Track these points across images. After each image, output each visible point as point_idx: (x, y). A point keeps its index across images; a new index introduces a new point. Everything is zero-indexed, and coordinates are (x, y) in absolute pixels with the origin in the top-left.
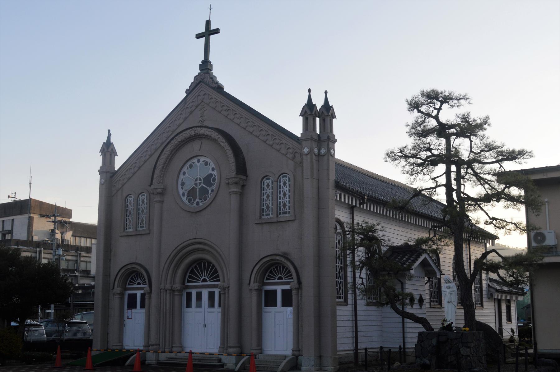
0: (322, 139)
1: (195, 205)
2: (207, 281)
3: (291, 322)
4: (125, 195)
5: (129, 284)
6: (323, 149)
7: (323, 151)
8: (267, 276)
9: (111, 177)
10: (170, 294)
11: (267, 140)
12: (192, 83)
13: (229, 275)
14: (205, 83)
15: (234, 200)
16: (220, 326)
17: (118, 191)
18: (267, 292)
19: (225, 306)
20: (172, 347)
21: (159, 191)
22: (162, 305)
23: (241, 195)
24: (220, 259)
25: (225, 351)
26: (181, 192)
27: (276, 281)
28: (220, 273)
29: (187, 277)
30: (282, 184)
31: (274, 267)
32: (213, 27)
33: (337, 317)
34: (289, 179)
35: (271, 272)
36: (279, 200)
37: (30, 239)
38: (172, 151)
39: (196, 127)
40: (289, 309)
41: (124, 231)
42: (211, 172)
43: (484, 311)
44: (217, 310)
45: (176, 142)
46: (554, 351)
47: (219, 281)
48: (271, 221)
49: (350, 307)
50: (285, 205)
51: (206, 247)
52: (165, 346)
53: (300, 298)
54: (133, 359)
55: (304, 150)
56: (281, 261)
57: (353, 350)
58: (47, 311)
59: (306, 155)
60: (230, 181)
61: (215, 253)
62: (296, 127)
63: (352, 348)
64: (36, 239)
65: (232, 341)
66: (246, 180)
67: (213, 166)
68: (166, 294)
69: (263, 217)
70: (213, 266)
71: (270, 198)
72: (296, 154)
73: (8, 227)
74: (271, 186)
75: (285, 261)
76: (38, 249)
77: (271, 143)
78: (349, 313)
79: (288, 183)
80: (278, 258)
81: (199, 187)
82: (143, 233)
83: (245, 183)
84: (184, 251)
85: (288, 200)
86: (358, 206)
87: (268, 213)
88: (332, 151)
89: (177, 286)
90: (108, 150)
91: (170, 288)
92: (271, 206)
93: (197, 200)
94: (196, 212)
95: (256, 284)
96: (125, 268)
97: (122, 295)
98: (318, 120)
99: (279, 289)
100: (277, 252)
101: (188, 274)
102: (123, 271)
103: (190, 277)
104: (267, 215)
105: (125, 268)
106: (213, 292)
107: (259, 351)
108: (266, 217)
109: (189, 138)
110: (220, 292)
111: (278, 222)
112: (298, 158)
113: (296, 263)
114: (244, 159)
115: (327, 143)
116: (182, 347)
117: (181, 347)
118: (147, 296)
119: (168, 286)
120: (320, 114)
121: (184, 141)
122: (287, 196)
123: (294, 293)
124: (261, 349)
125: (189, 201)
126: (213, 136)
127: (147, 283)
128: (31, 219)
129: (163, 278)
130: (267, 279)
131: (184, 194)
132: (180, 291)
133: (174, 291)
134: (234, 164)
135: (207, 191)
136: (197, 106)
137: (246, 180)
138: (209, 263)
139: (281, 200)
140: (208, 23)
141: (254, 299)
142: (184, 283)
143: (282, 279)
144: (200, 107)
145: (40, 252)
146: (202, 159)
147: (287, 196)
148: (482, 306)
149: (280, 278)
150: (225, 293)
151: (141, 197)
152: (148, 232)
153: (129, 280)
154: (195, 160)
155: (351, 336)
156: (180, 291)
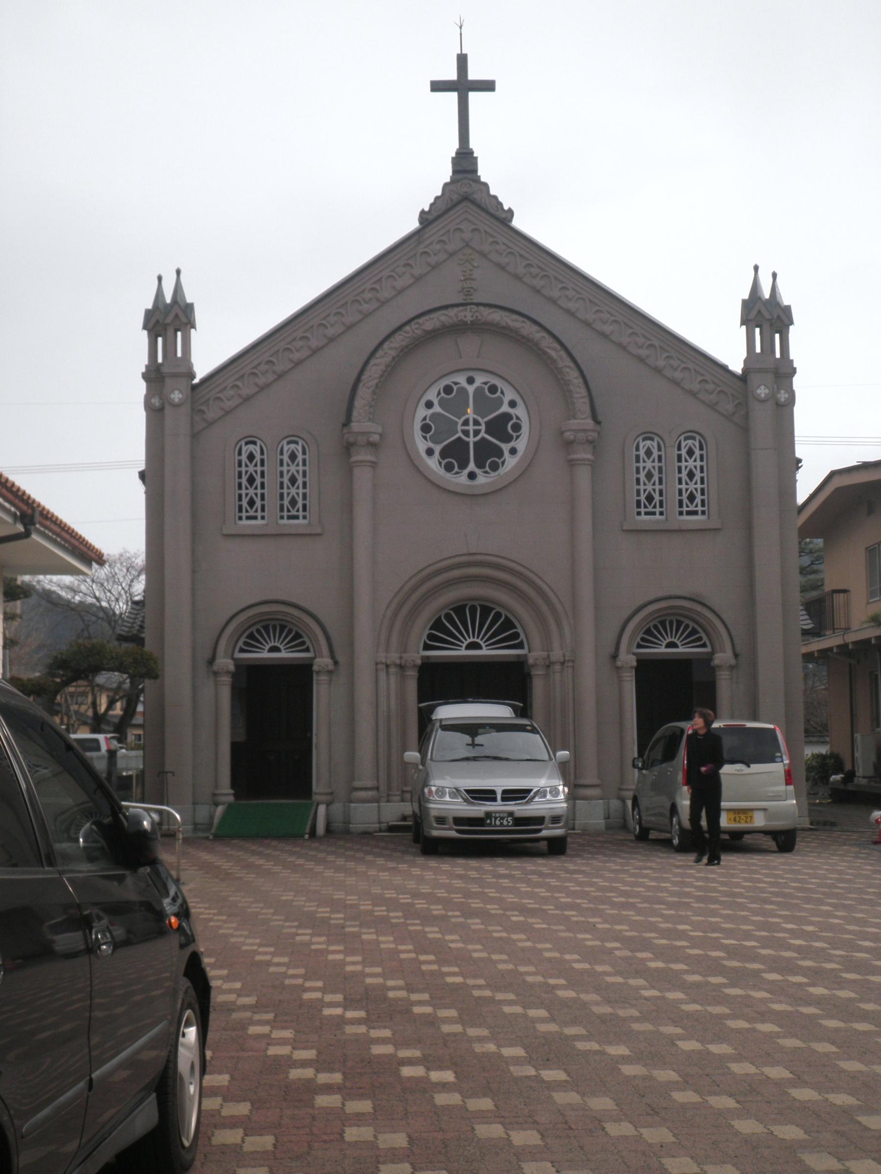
12: (437, 198)
14: (466, 202)
38: (402, 350)
45: (418, 332)
50: (692, 498)
55: (759, 391)
81: (472, 440)
90: (169, 319)
102: (663, 604)
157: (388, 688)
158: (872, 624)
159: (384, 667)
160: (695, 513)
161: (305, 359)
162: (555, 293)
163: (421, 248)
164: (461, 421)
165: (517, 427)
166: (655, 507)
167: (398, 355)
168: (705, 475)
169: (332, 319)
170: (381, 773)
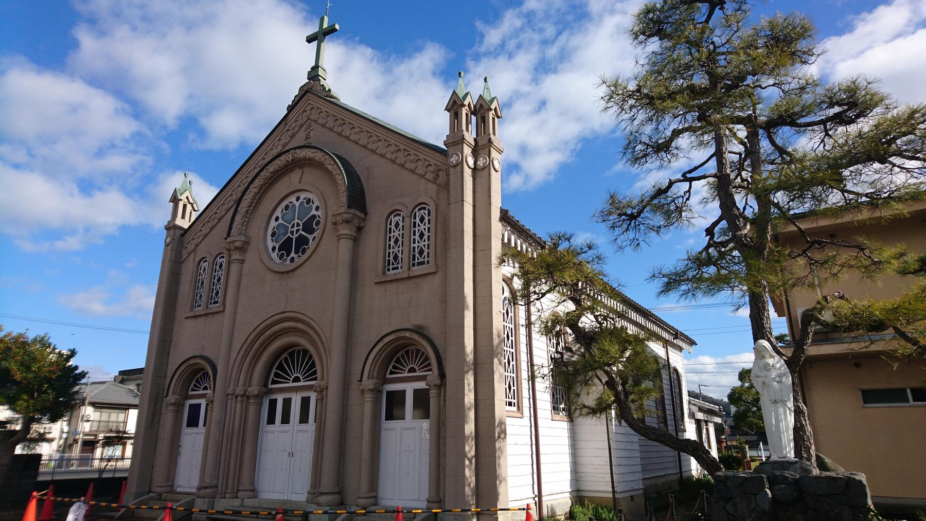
2: (300, 381)
3: (426, 445)
4: (198, 259)
5: (193, 390)
7: (481, 163)
8: (391, 367)
9: (182, 235)
10: (242, 402)
13: (331, 368)
15: (345, 247)
17: (189, 254)
18: (390, 394)
20: (238, 491)
21: (238, 244)
22: (227, 420)
23: (356, 240)
24: (319, 343)
26: (270, 245)
27: (406, 374)
28: (318, 367)
29: (272, 375)
30: (417, 220)
31: (402, 352)
35: (398, 361)
36: (412, 245)
38: (261, 188)
39: (295, 148)
41: (192, 310)
42: (314, 212)
46: (894, 501)
47: (315, 379)
49: (526, 421)
50: (421, 252)
51: (300, 326)
52: (226, 489)
53: (442, 403)
59: (455, 166)
60: (339, 218)
65: (327, 483)
67: (317, 203)
68: (236, 401)
69: (388, 273)
70: (311, 357)
71: (400, 242)
72: (441, 173)
75: (420, 340)
80: (408, 334)
82: (215, 310)
85: (426, 243)
87: (396, 266)
89: (254, 389)
91: (242, 393)
93: (293, 255)
94: (288, 272)
95: (371, 381)
97: (179, 406)
100: (408, 326)
101: (274, 371)
102: (182, 368)
103: (276, 375)
104: (393, 269)
106: (309, 398)
107: (372, 500)
108: (391, 272)
109: (286, 166)
111: (409, 278)
113: (437, 343)
114: (363, 190)
116: (254, 492)
117: (254, 491)
119: (239, 390)
120: (478, 107)
123: (433, 393)
124: (376, 497)
125: (281, 257)
126: (317, 158)
129: (233, 376)
131: (274, 249)
132: (260, 397)
133: (248, 397)
134: (345, 194)
135: (306, 241)
138: (306, 351)
139: (416, 245)
141: (368, 407)
142: (266, 385)
143: (415, 371)
144: (305, 126)
146: (303, 196)
147: (426, 237)
149: (412, 370)
151: (219, 260)
152: (221, 309)
154: (293, 199)
156: (260, 397)
160: (423, 263)
162: (347, 132)
165: (318, 223)
168: (412, 237)
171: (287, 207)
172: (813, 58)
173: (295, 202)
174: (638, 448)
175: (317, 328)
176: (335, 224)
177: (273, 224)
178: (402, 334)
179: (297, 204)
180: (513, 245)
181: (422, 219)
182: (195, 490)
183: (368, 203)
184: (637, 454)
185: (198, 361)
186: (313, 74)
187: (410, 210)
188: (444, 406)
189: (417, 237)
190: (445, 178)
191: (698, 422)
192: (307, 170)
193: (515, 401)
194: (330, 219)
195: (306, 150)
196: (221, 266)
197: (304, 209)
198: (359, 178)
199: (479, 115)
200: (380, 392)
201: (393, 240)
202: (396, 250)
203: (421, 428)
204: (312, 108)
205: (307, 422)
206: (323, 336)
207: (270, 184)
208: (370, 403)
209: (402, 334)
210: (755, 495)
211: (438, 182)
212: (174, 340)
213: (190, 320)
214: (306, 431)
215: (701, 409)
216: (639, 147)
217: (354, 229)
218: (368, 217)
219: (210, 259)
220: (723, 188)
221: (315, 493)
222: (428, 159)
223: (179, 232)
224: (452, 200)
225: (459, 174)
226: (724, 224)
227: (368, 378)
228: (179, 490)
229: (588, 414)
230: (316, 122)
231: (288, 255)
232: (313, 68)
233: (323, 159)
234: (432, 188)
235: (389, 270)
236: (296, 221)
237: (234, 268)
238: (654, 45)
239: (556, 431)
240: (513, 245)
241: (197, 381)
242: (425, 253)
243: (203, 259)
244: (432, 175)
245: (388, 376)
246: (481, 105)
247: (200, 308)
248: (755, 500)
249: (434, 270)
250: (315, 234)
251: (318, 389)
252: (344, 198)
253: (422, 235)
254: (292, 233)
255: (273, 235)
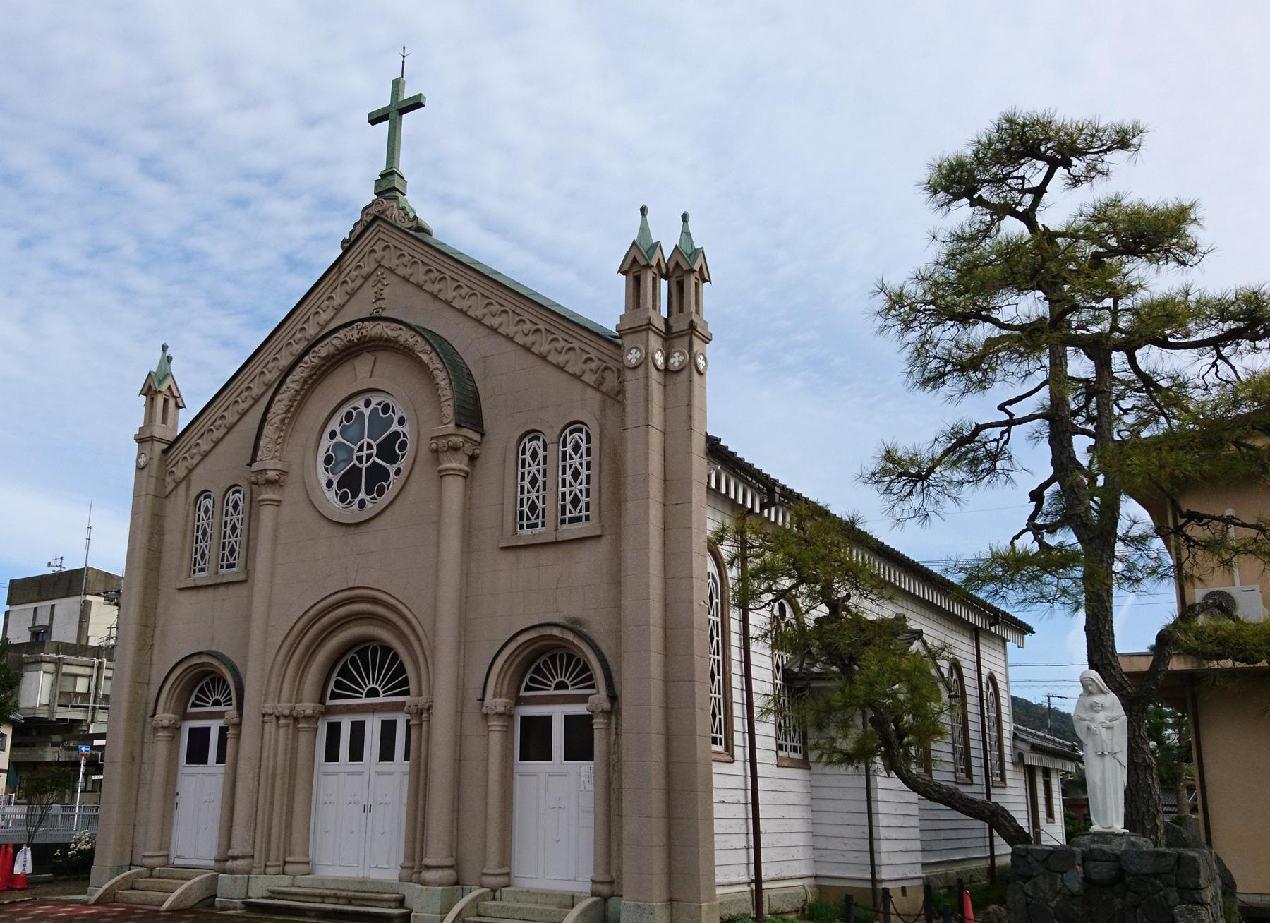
0: (674, 330)
1: (355, 507)
2: (378, 695)
4: (193, 494)
5: (194, 705)
6: (677, 355)
7: (676, 361)
8: (526, 680)
9: (165, 452)
11: (533, 343)
13: (442, 679)
14: (386, 224)
16: (404, 809)
17: (178, 484)
18: (526, 720)
19: (419, 757)
20: (285, 863)
25: (415, 876)
27: (552, 692)
28: (411, 674)
32: (408, 93)
33: (715, 791)
34: (588, 434)
35: (538, 671)
36: (561, 490)
37: (83, 642)
38: (305, 382)
39: (363, 320)
40: (583, 768)
42: (395, 427)
43: (1008, 791)
44: (400, 764)
47: (407, 693)
48: (540, 541)
49: (739, 767)
50: (575, 502)
51: (380, 610)
52: (268, 859)
54: (182, 893)
55: (630, 357)
56: (566, 640)
57: (749, 884)
58: (95, 777)
59: (635, 368)
61: (399, 622)
62: (604, 304)
63: (746, 879)
64: (93, 642)
66: (480, 444)
68: (278, 726)
69: (520, 532)
70: (396, 656)
71: (540, 484)
73: (43, 620)
74: (540, 457)
75: (576, 641)
76: (96, 661)
77: (545, 348)
78: (739, 782)
79: (584, 446)
80: (556, 632)
81: (365, 465)
83: (477, 451)
84: (326, 620)
85: (584, 487)
86: (757, 510)
87: (533, 521)
88: (700, 361)
90: (158, 391)
92: (540, 505)
93: (362, 495)
94: (357, 525)
96: (185, 666)
98: (664, 284)
99: (558, 714)
101: (334, 678)
102: (513, 646)
103: (338, 685)
104: (529, 526)
105: (185, 666)
108: (527, 531)
110: (408, 721)
112: (611, 381)
115: (686, 339)
117: (308, 863)
118: (231, 732)
121: (334, 356)
122: (583, 477)
123: (598, 723)
124: (508, 874)
125: (343, 499)
126: (401, 340)
127: (234, 702)
128: (86, 606)
130: (528, 688)
131: (329, 484)
135: (385, 475)
136: (366, 278)
137: (480, 444)
138: (387, 649)
139: (567, 489)
140: (397, 85)
141: (496, 739)
144: (374, 278)
145: (100, 667)
146: (376, 400)
147: (583, 477)
148: (1003, 779)
150: (420, 725)
153: (195, 693)
154: (360, 403)
155: (744, 844)
157: (276, 742)
158: (613, 718)
159: (273, 718)
160: (578, 519)
161: (248, 410)
162: (449, 294)
163: (341, 279)
164: (356, 448)
165: (403, 446)
166: (537, 518)
167: (302, 389)
168: (561, 477)
169: (271, 365)
170: (258, 841)
171: (349, 416)
172: (1196, 259)
173: (363, 408)
174: (916, 812)
175: (409, 616)
176: (435, 451)
177: (326, 442)
178: (548, 631)
179: (367, 412)
180: (724, 491)
181: (576, 448)
182: (212, 863)
183: (484, 417)
184: (915, 822)
185: (205, 659)
186: (385, 185)
187: (558, 432)
188: (617, 743)
189: (568, 476)
190: (616, 383)
191: (1030, 771)
192: (382, 356)
193: (722, 736)
194: (426, 444)
195: (383, 324)
196: (236, 506)
197: (379, 423)
198: (470, 374)
199: (674, 280)
200: (511, 717)
201: (527, 479)
202: (533, 495)
203: (579, 774)
204: (387, 247)
205: (392, 759)
206: (418, 628)
207: (320, 376)
208: (498, 734)
209: (548, 631)
210: (1062, 873)
211: (604, 388)
212: (160, 623)
213: (187, 594)
214: (360, 774)
215: (1035, 748)
216: (934, 364)
217: (466, 459)
218: (486, 439)
219: (216, 493)
220: (1059, 426)
221: (415, 866)
222: (588, 348)
223: (159, 447)
224: (630, 422)
225: (642, 381)
226: (1056, 486)
227: (495, 697)
228: (178, 862)
229: (840, 762)
230: (392, 271)
231: (354, 496)
232: (383, 176)
233: (411, 341)
234: (593, 397)
235: (521, 527)
236: (366, 440)
237: (267, 513)
238: (963, 215)
239: (783, 787)
240: (724, 491)
241: (201, 691)
242: (582, 504)
243: (204, 493)
244: (594, 377)
245: (522, 693)
246: (677, 264)
247: (203, 574)
248: (1062, 879)
249: (598, 532)
250: (401, 464)
251: (413, 709)
252: (449, 411)
253: (576, 474)
254: (360, 459)
255: (328, 460)
